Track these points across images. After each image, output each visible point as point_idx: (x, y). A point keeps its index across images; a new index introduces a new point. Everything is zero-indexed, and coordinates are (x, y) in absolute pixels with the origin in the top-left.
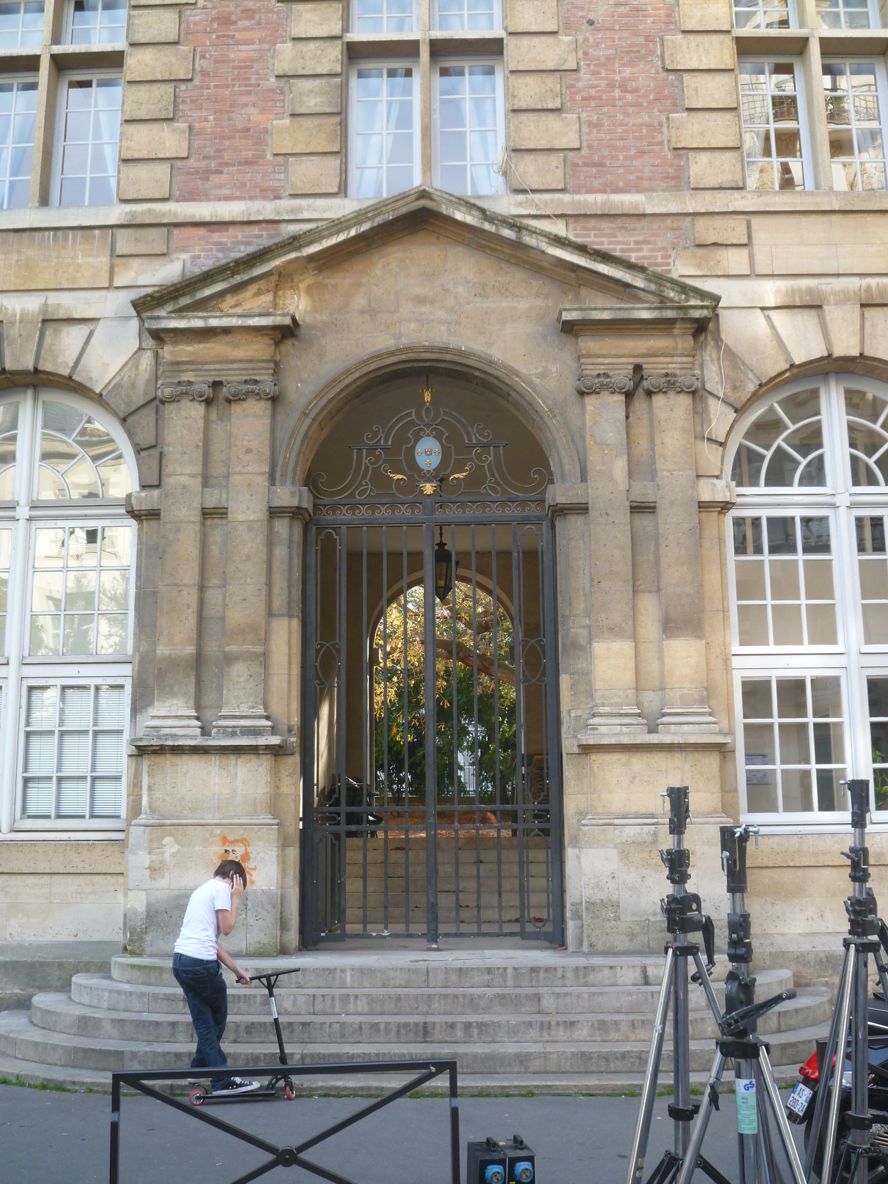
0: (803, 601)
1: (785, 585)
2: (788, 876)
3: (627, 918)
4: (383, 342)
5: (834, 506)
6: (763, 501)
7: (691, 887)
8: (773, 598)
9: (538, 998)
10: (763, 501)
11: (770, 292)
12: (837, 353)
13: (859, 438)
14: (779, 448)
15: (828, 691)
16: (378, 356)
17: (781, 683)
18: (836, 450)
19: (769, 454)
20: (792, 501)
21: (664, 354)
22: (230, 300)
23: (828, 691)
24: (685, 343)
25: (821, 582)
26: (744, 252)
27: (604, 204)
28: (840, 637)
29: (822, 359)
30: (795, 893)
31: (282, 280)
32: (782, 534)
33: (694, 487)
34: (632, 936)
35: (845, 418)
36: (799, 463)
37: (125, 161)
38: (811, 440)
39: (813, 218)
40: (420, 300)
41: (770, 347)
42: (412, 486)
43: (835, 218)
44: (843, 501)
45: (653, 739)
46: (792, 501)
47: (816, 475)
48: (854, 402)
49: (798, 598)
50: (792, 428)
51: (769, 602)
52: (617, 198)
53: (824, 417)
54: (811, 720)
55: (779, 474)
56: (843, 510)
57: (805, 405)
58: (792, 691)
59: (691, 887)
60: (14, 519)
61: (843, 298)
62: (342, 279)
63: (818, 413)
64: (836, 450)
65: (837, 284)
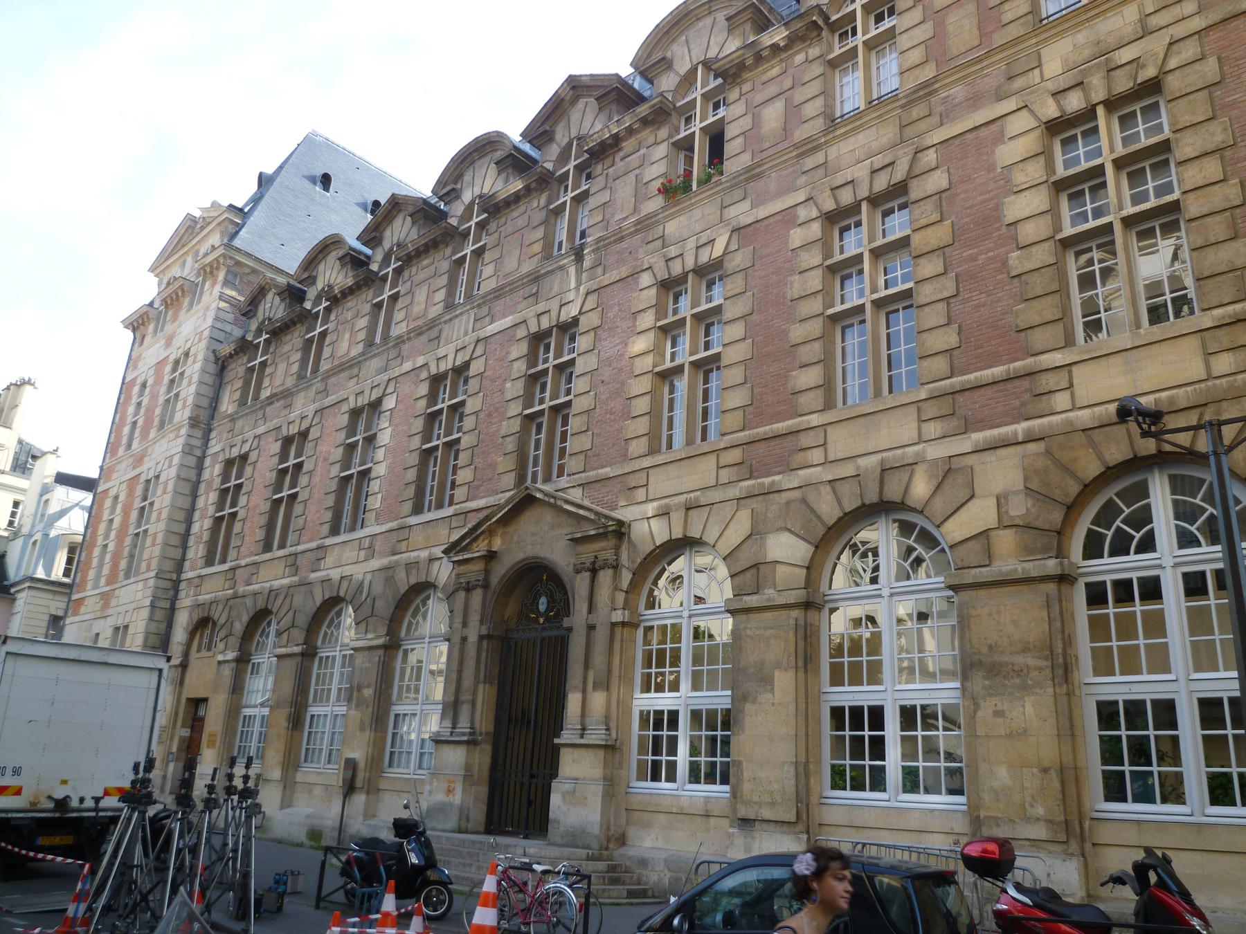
0: (1141, 641)
1: (1126, 629)
2: (646, 816)
3: (562, 828)
4: (521, 556)
5: (1160, 567)
6: (1109, 568)
7: (151, 776)
8: (1118, 640)
9: (478, 855)
10: (1109, 568)
11: (650, 509)
12: (867, 502)
13: (1184, 513)
14: (1118, 528)
15: (1166, 712)
16: (517, 563)
17: (870, 708)
18: (1164, 523)
19: (1110, 534)
20: (1131, 566)
21: (604, 550)
22: (475, 545)
23: (1166, 712)
24: (612, 542)
25: (1156, 625)
26: (1068, 392)
27: (1008, 371)
28: (1173, 669)
29: (858, 508)
30: (647, 825)
31: (490, 532)
32: (1124, 590)
33: (610, 615)
34: (563, 837)
35: (1169, 497)
36: (1134, 537)
37: (1198, 280)
38: (1143, 518)
39: (670, 466)
40: (533, 535)
41: (649, 539)
42: (536, 621)
43: (683, 462)
44: (1168, 562)
45: (583, 741)
46: (1131, 566)
47: (1148, 544)
48: (1178, 485)
49: (1137, 639)
50: (1127, 511)
51: (1141, 641)
52: (600, 471)
53: (1152, 500)
54: (847, 733)
55: (1121, 547)
56: (1169, 571)
57: (1141, 491)
58: (1135, 710)
59: (151, 776)
60: (880, 596)
61: (678, 507)
62: (511, 529)
63: (1148, 497)
64: (1164, 523)
65: (677, 500)
